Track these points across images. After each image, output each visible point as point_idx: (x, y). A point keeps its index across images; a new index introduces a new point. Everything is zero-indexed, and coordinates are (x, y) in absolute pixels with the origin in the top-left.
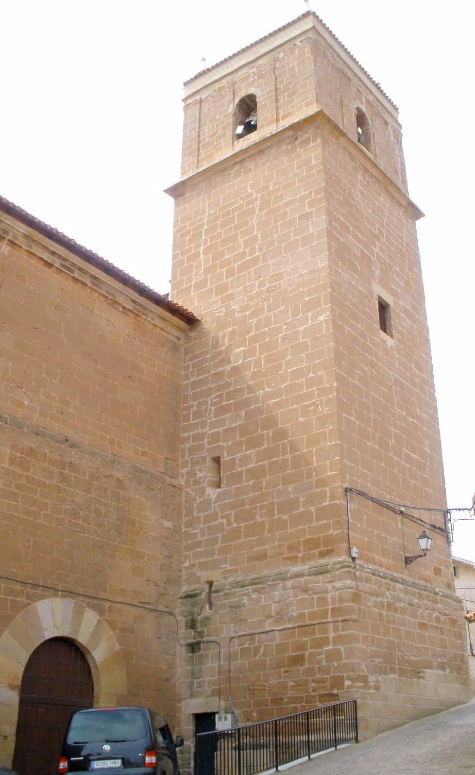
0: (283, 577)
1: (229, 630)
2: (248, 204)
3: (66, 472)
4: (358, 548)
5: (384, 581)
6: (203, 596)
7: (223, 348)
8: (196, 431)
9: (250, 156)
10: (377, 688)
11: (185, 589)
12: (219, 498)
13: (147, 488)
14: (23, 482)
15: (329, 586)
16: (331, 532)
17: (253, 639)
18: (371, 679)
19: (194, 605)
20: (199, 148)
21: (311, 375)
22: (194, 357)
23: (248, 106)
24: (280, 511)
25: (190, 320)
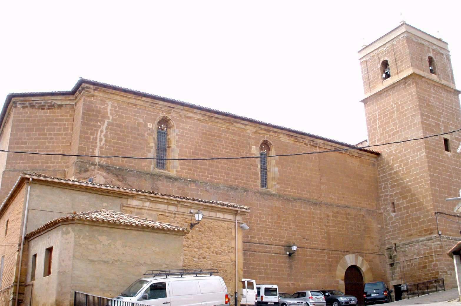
0: (418, 242)
1: (403, 259)
2: (392, 109)
3: (348, 216)
4: (441, 231)
5: (451, 240)
6: (393, 248)
7: (391, 164)
8: (385, 194)
9: (390, 89)
10: (451, 275)
11: (387, 246)
12: (395, 216)
13: (372, 216)
14: (336, 222)
15: (433, 244)
16: (432, 227)
17: (410, 261)
18: (449, 272)
19: (391, 251)
20: (369, 82)
21: (421, 175)
22: (381, 167)
23: (385, 64)
24: (416, 220)
25: (378, 154)
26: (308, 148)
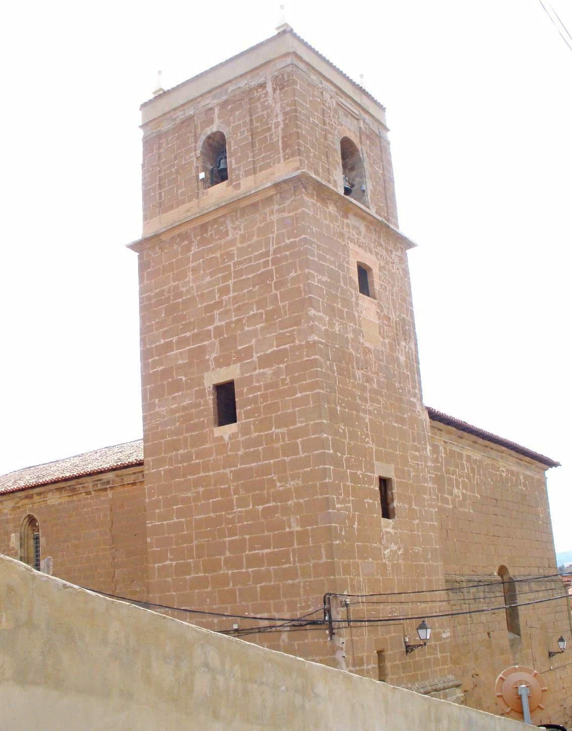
26: (92, 498)
